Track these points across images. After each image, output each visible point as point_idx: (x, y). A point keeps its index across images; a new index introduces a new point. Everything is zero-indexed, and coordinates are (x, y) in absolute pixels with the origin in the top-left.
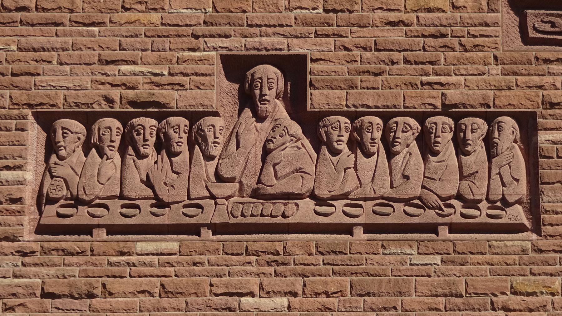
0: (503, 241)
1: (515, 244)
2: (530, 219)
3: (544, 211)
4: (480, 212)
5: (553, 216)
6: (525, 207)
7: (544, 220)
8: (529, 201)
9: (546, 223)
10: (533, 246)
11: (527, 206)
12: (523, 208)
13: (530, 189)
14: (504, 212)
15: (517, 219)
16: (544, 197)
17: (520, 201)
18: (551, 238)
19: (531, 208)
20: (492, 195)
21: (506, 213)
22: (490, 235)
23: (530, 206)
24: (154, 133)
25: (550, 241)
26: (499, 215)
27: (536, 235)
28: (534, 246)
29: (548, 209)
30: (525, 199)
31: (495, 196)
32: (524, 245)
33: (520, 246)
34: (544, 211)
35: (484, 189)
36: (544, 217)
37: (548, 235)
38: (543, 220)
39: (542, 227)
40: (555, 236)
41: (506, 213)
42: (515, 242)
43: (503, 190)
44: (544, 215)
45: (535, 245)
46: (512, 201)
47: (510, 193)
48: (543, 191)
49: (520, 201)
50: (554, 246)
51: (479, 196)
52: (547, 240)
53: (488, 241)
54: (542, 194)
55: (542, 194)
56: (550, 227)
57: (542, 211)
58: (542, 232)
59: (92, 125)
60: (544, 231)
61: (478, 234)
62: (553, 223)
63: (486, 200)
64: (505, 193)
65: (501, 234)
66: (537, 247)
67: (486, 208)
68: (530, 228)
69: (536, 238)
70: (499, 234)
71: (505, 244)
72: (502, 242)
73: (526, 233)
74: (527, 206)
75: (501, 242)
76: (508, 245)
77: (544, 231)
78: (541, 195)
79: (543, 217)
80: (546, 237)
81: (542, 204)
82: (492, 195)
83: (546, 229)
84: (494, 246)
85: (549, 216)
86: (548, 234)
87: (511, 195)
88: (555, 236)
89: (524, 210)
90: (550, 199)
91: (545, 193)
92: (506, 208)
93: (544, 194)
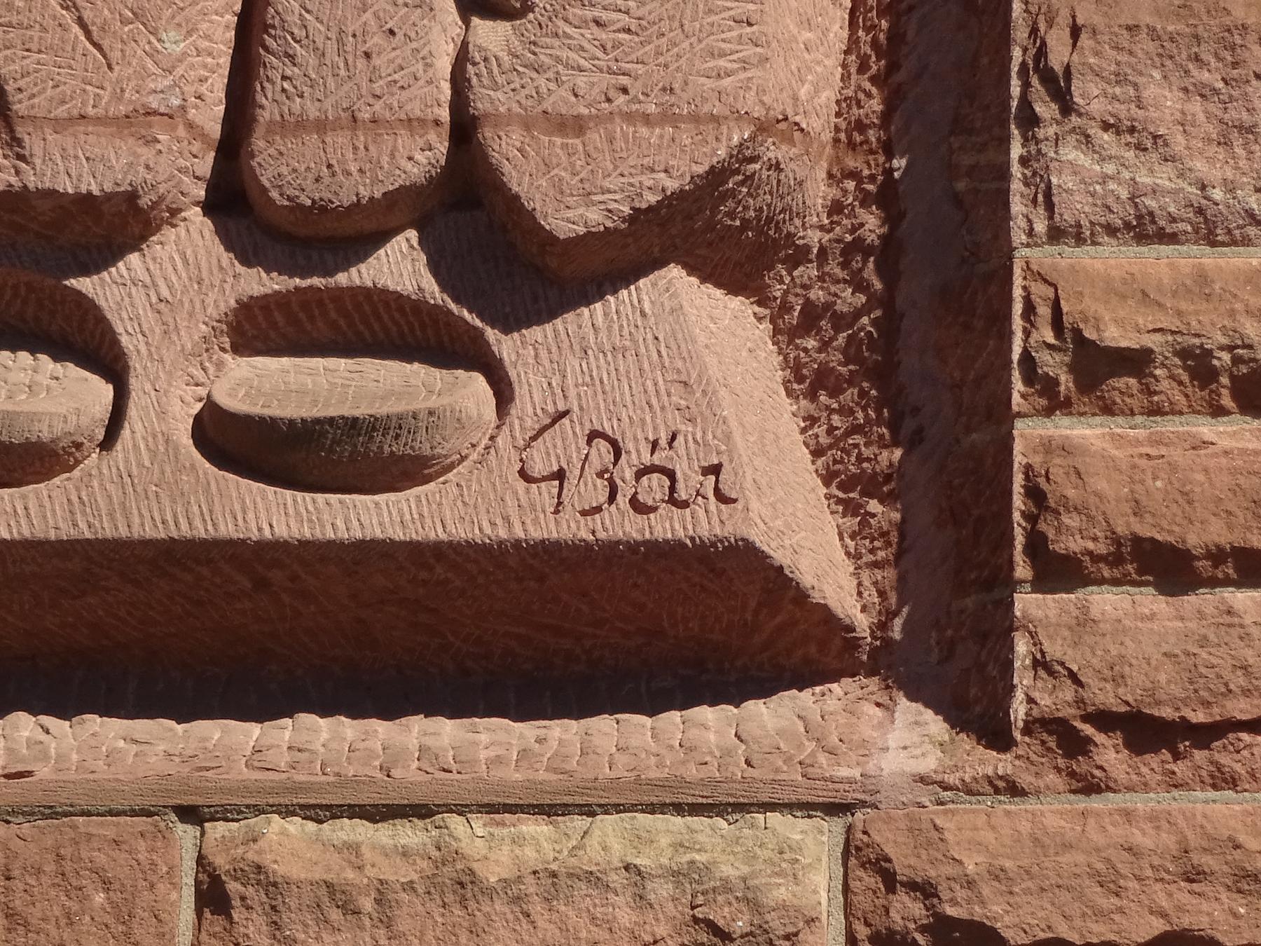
0: (420, 812)
1: (592, 856)
2: (871, 485)
3: (1053, 364)
4: (106, 391)
5: (1206, 428)
6: (811, 317)
7: (1062, 487)
8: (872, 224)
9: (1074, 544)
10: (866, 880)
11: (849, 299)
12: (785, 334)
13: (892, 49)
14: (479, 382)
15: (655, 486)
16: (1071, 153)
17: (727, 216)
18: (1155, 761)
19: (890, 326)
20: (300, 125)
21: (503, 393)
22: (252, 732)
23: (886, 301)
24: (32, 113)
25: (1140, 803)
26: (353, 424)
27: (936, 725)
28: (890, 881)
29: (1115, 336)
30: (819, 192)
31: (339, 140)
32: (730, 869)
33: (661, 890)
34: (1053, 364)
35: (173, 44)
36: (1066, 449)
37: (1104, 720)
38: (1035, 494)
39: (1026, 603)
40: (1206, 735)
41: (503, 393)
42: (607, 822)
43: (462, 58)
44: (1064, 427)
45: (904, 862)
46: (595, 217)
47: (559, 101)
48: (1058, 56)
49: (727, 216)
50: (1194, 876)
51: (96, 142)
52: (1090, 787)
53: (190, 814)
54: (1045, 109)
55: (1045, 109)
56: (1149, 600)
57: (1028, 360)
58: (1023, 679)
59: (673, 262)
60: (1041, 664)
61: (65, 712)
62: (1194, 540)
63: (210, 207)
64: (483, 99)
65: (603, 725)
66: (925, 890)
67: (194, 331)
68: (863, 623)
69: (929, 763)
70: (389, 712)
71: (447, 855)
72: (410, 834)
73: (805, 698)
74: (849, 299)
75: (384, 834)
76: (492, 875)
77: (1041, 664)
78: (1029, 120)
79: (1048, 447)
80: (1074, 745)
81: (1045, 256)
82: (300, 125)
83: (1084, 621)
84: (271, 885)
85: (1137, 429)
86: (1106, 697)
87: (574, 126)
88: (1206, 735)
89: (796, 370)
90: (1164, 177)
91: (1085, 91)
92: (508, 325)
93: (1067, 108)
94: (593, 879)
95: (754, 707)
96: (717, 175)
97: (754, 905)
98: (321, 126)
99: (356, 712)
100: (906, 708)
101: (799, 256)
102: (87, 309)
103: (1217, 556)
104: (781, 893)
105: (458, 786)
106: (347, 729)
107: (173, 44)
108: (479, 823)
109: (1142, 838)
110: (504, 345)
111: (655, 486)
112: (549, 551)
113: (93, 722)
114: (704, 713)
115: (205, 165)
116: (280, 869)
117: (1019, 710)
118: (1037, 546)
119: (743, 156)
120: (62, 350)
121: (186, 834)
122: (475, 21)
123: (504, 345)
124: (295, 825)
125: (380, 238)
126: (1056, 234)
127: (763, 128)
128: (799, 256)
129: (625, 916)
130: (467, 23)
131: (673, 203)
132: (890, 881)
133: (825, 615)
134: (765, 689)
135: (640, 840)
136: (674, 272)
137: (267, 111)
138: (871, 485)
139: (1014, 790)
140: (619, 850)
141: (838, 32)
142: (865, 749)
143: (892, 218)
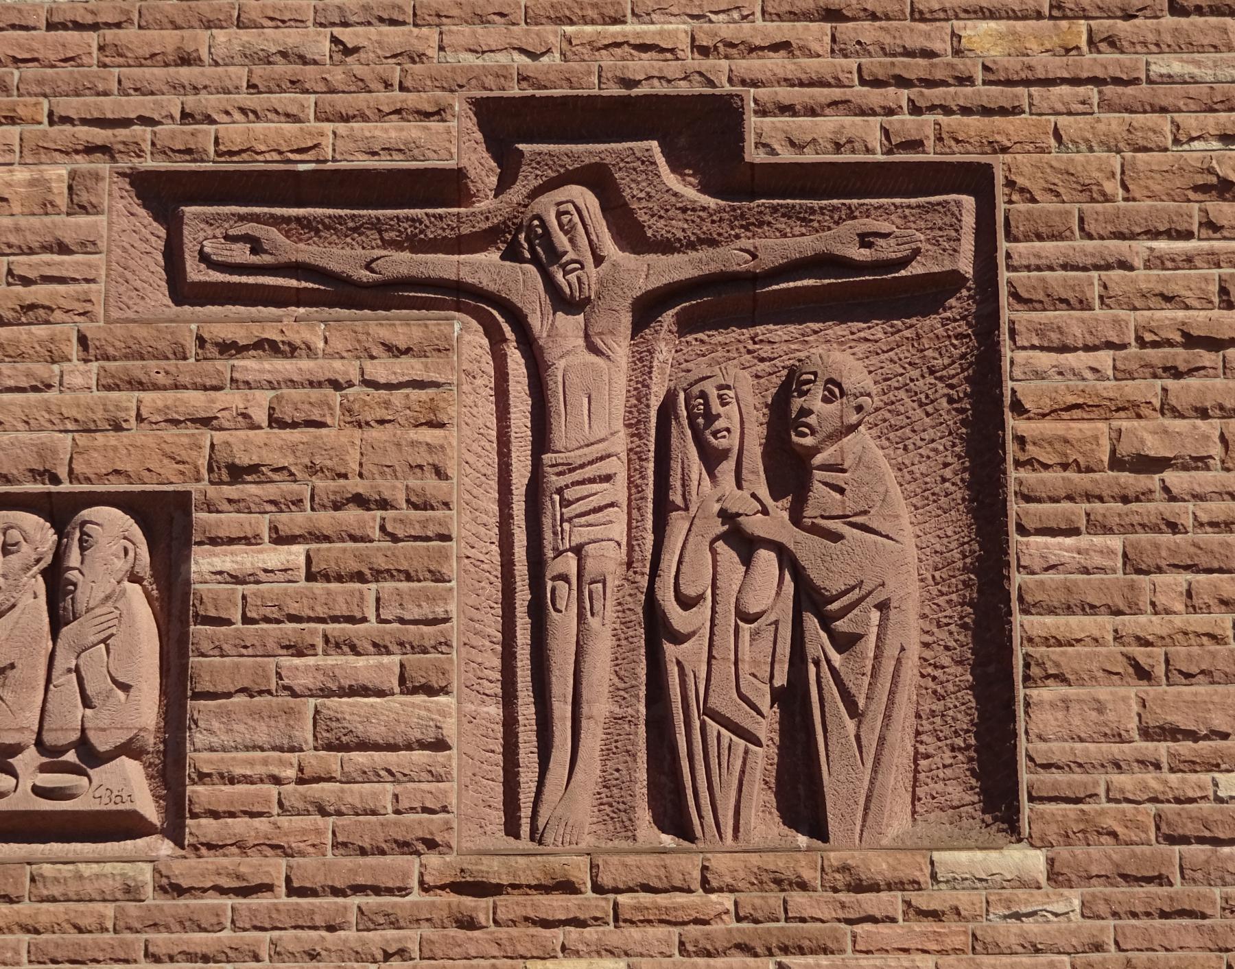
0: (73, 863)
1: (105, 871)
2: (160, 797)
3: (194, 776)
5: (223, 787)
6: (151, 764)
7: (195, 799)
8: (162, 747)
9: (197, 810)
10: (157, 875)
11: (157, 761)
12: (146, 768)
13: (166, 713)
16: (198, 735)
18: (212, 852)
22: (42, 846)
23: (164, 762)
25: (210, 860)
26: (61, 788)
27: (172, 844)
28: (162, 876)
29: (206, 770)
30: (152, 741)
31: (59, 733)
32: (131, 874)
34: (194, 776)
37: (202, 844)
39: (188, 821)
42: (108, 864)
45: (164, 872)
47: (101, 725)
50: (219, 874)
51: (13, 734)
52: (200, 857)
53: (29, 864)
54: (193, 726)
55: (193, 726)
56: (211, 821)
58: (187, 836)
62: (220, 809)
64: (87, 725)
65: (109, 844)
66: (168, 877)
68: (159, 825)
69: (169, 853)
71: (78, 871)
72: (71, 867)
73: (147, 839)
74: (157, 761)
76: (86, 875)
78: (190, 729)
79: (193, 792)
80: (197, 849)
83: (199, 825)
85: (209, 788)
86: (203, 840)
87: (104, 730)
89: (147, 775)
90: (215, 739)
91: (200, 723)
92: (92, 768)
94: (105, 876)
95: (138, 841)
96: (131, 739)
97: (135, 880)
98: (56, 730)
99: (62, 842)
100: (167, 841)
101: (148, 753)
102: (11, 765)
103: (224, 812)
104: (140, 878)
105: (80, 857)
106: (60, 845)
107: (28, 714)
108: (84, 865)
109: (210, 867)
110: (90, 772)
111: (119, 799)
112: (98, 812)
113: (12, 845)
114: (128, 842)
115: (34, 737)
116: (46, 874)
117: (186, 843)
118: (190, 810)
119: (136, 735)
120: (7, 773)
121: (28, 867)
122: (559, 314)
123: (90, 772)
124: (49, 866)
125: (67, 751)
126: (195, 750)
127: (140, 730)
128: (148, 753)
129: (111, 882)
130: (554, 314)
131: (123, 745)
132: (162, 876)
133: (151, 823)
134: (140, 837)
135: (114, 868)
136: (123, 757)
137: (46, 726)
138: (160, 797)
139: (185, 858)
140: (110, 870)
141: (156, 709)
142: (158, 849)
143: (165, 746)
